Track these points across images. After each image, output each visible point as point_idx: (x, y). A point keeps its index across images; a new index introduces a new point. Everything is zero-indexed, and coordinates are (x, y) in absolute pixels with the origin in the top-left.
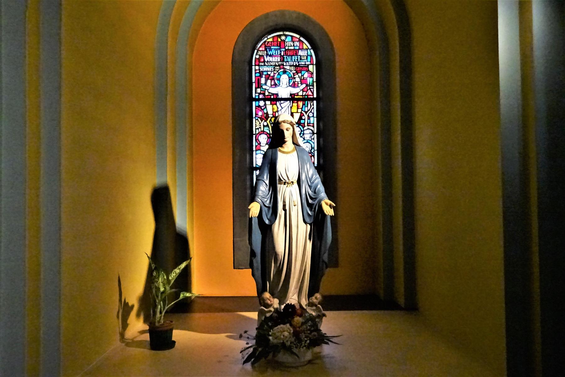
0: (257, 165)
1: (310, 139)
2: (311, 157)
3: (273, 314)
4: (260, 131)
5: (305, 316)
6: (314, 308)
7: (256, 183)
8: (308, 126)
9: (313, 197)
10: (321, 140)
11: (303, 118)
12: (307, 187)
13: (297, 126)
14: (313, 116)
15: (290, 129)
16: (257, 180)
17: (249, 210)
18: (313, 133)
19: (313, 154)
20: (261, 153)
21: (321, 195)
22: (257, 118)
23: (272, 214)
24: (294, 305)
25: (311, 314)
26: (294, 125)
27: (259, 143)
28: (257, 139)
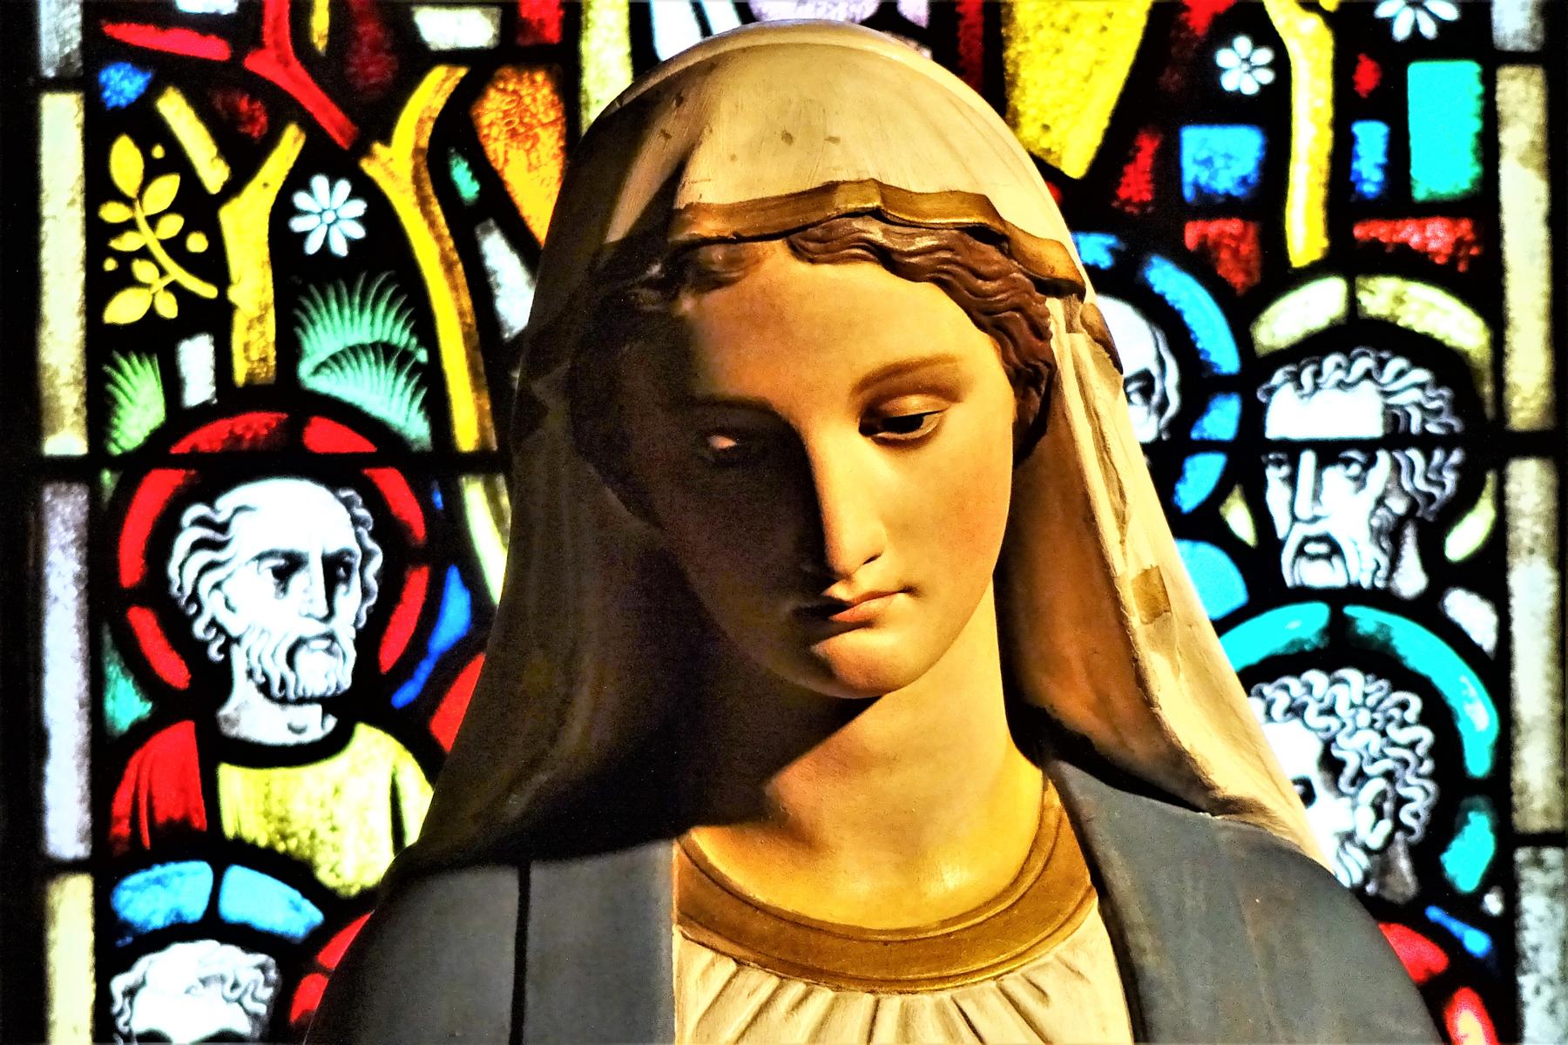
1: (1411, 580)
4: (199, 388)
15: (949, 393)
19: (1476, 942)
20: (232, 909)
22: (123, 84)
27: (174, 671)
28: (131, 569)
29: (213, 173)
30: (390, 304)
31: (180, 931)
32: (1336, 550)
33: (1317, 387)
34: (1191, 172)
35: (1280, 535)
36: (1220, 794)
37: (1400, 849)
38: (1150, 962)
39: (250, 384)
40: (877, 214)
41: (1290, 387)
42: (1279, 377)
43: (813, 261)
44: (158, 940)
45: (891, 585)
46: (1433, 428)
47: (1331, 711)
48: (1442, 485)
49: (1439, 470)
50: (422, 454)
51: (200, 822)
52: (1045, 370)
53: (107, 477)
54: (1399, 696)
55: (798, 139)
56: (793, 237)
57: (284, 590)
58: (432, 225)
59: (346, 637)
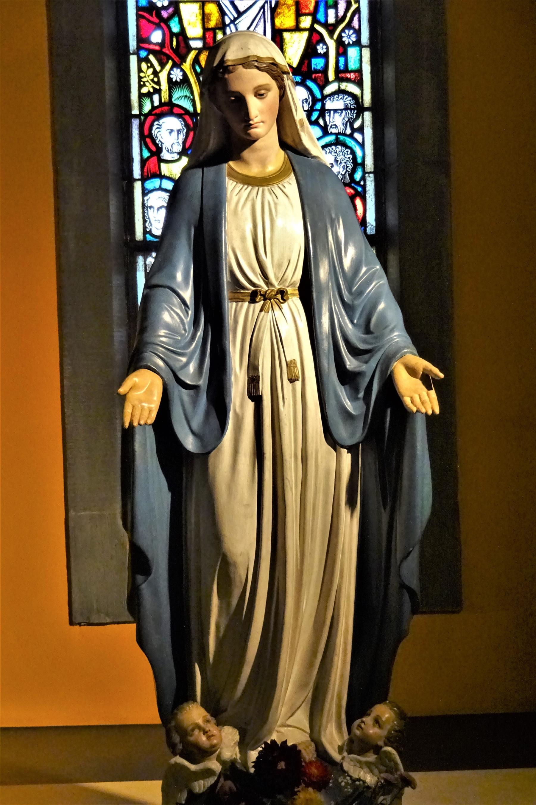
0: (150, 233)
1: (348, 131)
2: (352, 198)
3: (217, 782)
4: (156, 103)
5: (337, 784)
6: (371, 757)
7: (145, 297)
8: (339, 79)
9: (361, 346)
10: (390, 134)
11: (321, 49)
12: (338, 308)
13: (297, 84)
14: (358, 43)
15: (268, 90)
16: (148, 286)
17: (123, 398)
18: (360, 109)
19: (359, 189)
20: (163, 186)
21: (392, 339)
22: (143, 54)
23: (207, 414)
24: (294, 746)
25: (359, 780)
26: (285, 76)
27: (153, 148)
28: (146, 132)
29: (158, 68)
30: (187, 89)
31: (155, 190)
32: (336, 127)
33: (333, 100)
34: (313, 66)
35: (328, 125)
36: (312, 155)
37: (347, 174)
38: (302, 182)
39: (165, 103)
40: (256, 61)
41: (329, 100)
42: (327, 99)
43: (246, 69)
44: (151, 191)
45: (260, 121)
46: (352, 107)
47: (336, 152)
48: (354, 116)
49: (353, 114)
50: (192, 113)
51: (158, 173)
52: (284, 87)
53: (142, 117)
54: (347, 150)
55: (243, 48)
56: (244, 65)
57: (171, 135)
58: (193, 76)
59: (181, 143)
